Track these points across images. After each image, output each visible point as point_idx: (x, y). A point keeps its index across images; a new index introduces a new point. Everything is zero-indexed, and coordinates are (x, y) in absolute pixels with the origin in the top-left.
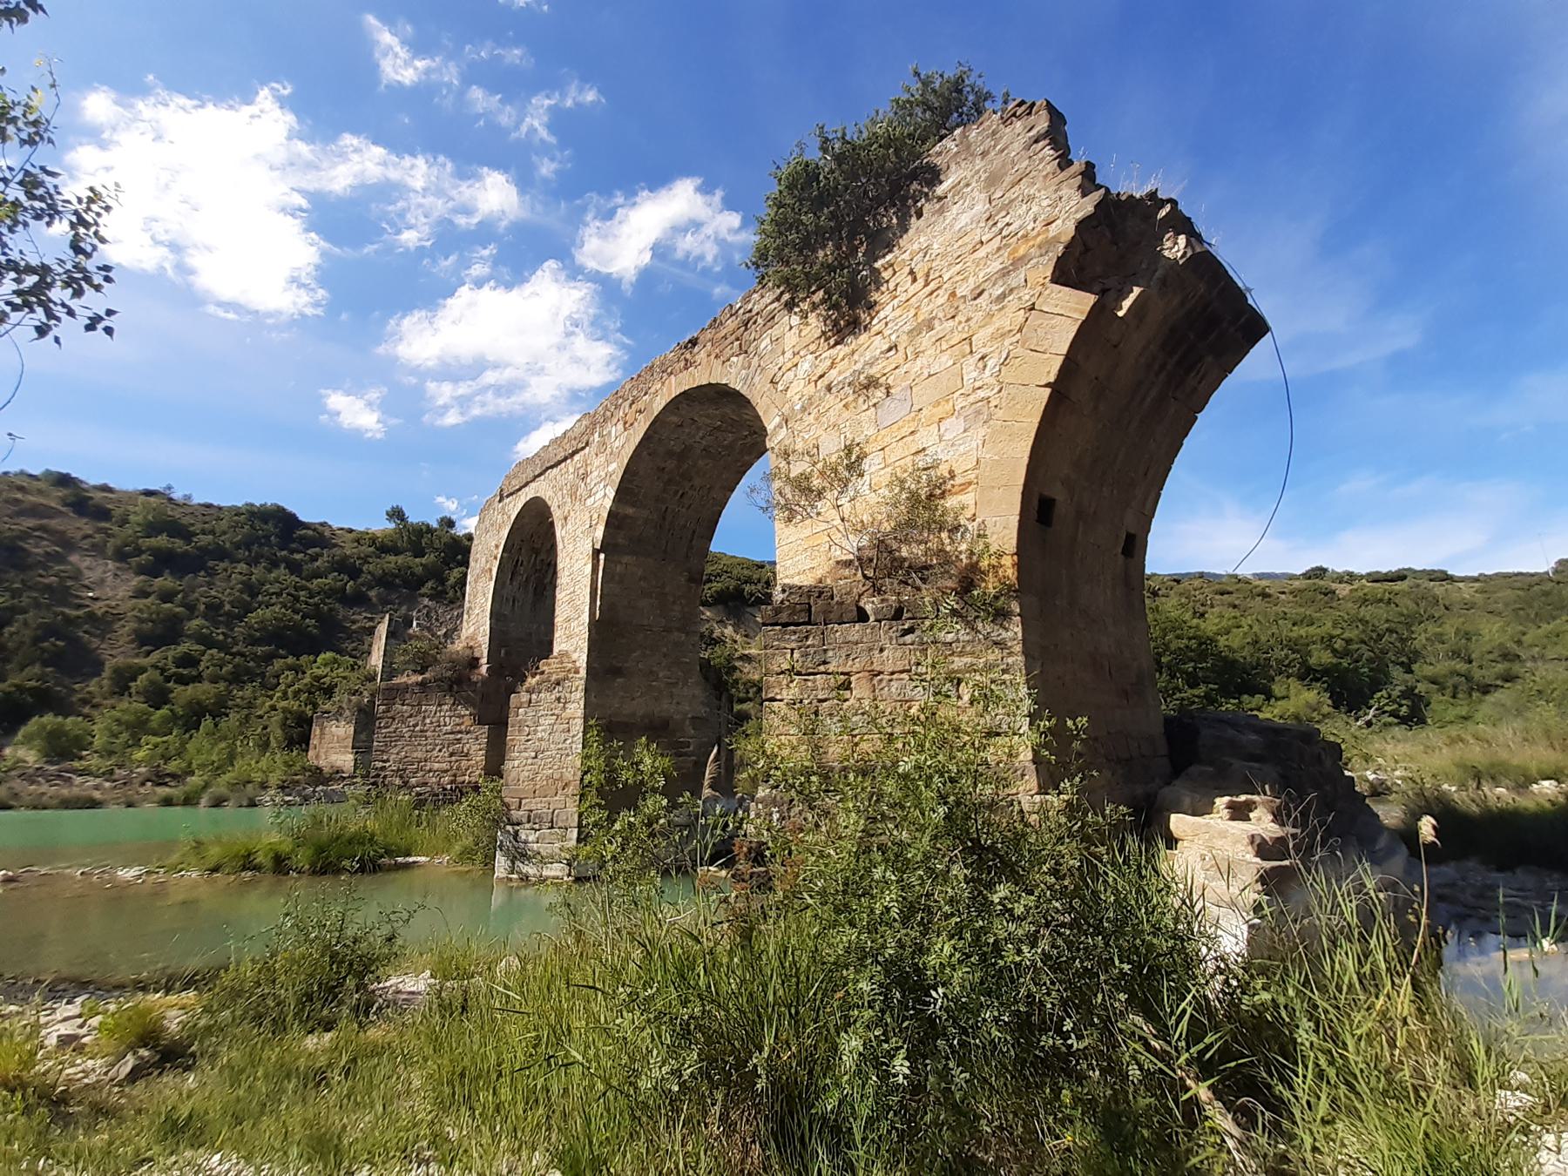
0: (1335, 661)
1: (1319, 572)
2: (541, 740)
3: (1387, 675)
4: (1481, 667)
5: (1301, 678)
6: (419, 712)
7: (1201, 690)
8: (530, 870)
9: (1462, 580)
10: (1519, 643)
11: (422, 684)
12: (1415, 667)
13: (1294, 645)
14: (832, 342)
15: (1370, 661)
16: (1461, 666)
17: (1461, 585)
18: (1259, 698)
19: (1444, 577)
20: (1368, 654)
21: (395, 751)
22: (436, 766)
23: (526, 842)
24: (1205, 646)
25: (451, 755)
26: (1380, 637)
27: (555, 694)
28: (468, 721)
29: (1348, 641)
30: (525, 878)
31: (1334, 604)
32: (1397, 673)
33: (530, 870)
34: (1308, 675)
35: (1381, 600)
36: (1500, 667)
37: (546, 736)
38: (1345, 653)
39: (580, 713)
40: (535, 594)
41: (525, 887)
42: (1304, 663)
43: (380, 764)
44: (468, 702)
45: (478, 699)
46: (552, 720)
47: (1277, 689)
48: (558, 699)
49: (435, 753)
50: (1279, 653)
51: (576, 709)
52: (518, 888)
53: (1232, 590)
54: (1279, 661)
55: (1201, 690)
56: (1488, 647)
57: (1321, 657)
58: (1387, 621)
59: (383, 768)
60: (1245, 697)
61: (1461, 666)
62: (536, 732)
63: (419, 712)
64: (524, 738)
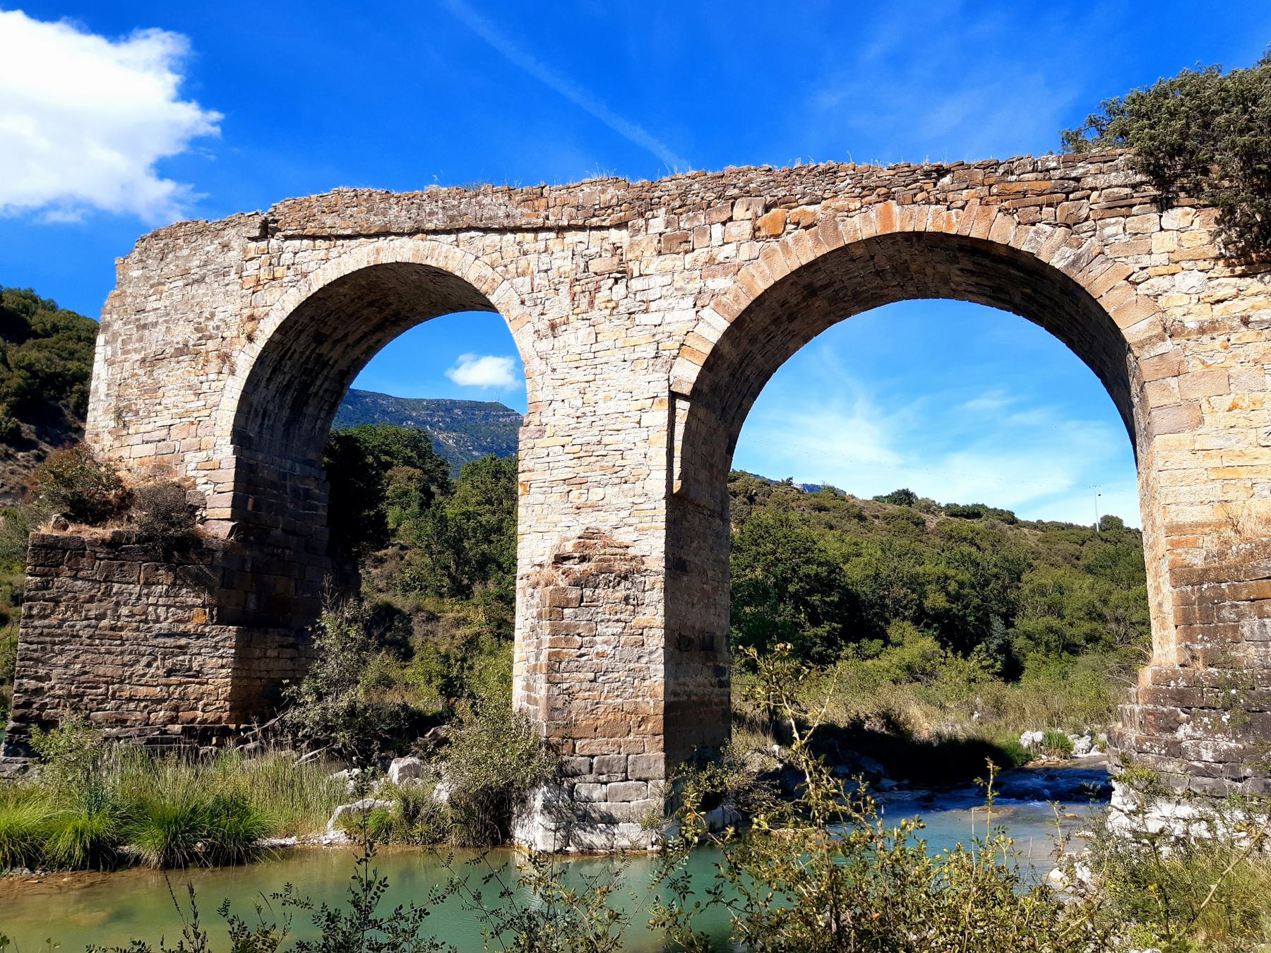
0: (947, 605)
1: (905, 497)
2: (601, 655)
3: (989, 624)
4: (1071, 625)
5: (916, 621)
6: (107, 593)
7: (823, 630)
8: (596, 839)
9: (1027, 524)
10: (1105, 602)
11: (114, 544)
12: (1017, 621)
13: (916, 584)
14: (1238, 270)
15: (978, 608)
16: (1054, 622)
17: (1026, 530)
18: (878, 643)
19: (1010, 519)
20: (977, 601)
21: (62, 660)
22: (142, 692)
23: (588, 800)
24: (828, 581)
25: (170, 673)
26: (987, 583)
27: (621, 593)
28: (197, 619)
29: (962, 585)
30: (590, 851)
31: (924, 538)
32: (997, 624)
33: (596, 839)
34: (922, 619)
35: (965, 539)
36: (1087, 627)
37: (609, 650)
38: (954, 598)
39: (659, 620)
40: (292, 408)
41: (590, 862)
42: (920, 606)
43: (32, 684)
44: (200, 583)
45: (216, 579)
46: (617, 628)
47: (893, 633)
48: (627, 599)
49: (139, 669)
50: (899, 591)
51: (653, 614)
52: (578, 865)
53: (827, 502)
54: (897, 601)
55: (823, 630)
56: (1080, 605)
57: (936, 600)
58: (995, 565)
59: (38, 692)
60: (865, 641)
61: (1054, 622)
62: (592, 644)
63: (107, 593)
64: (574, 652)
